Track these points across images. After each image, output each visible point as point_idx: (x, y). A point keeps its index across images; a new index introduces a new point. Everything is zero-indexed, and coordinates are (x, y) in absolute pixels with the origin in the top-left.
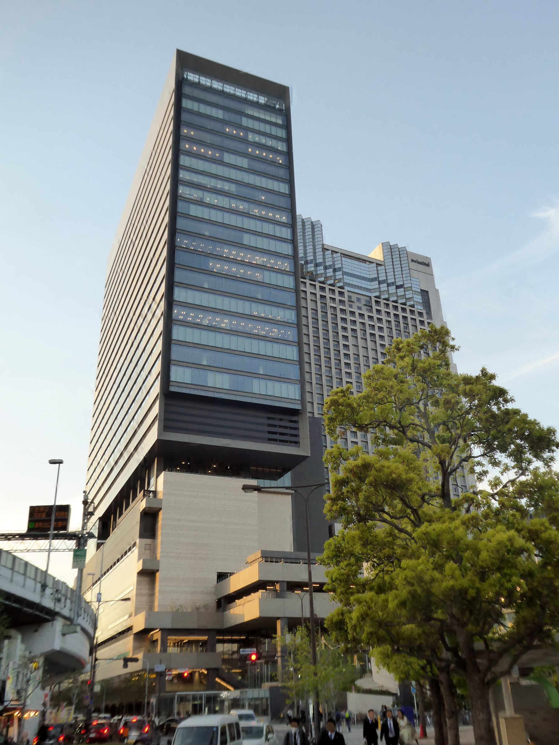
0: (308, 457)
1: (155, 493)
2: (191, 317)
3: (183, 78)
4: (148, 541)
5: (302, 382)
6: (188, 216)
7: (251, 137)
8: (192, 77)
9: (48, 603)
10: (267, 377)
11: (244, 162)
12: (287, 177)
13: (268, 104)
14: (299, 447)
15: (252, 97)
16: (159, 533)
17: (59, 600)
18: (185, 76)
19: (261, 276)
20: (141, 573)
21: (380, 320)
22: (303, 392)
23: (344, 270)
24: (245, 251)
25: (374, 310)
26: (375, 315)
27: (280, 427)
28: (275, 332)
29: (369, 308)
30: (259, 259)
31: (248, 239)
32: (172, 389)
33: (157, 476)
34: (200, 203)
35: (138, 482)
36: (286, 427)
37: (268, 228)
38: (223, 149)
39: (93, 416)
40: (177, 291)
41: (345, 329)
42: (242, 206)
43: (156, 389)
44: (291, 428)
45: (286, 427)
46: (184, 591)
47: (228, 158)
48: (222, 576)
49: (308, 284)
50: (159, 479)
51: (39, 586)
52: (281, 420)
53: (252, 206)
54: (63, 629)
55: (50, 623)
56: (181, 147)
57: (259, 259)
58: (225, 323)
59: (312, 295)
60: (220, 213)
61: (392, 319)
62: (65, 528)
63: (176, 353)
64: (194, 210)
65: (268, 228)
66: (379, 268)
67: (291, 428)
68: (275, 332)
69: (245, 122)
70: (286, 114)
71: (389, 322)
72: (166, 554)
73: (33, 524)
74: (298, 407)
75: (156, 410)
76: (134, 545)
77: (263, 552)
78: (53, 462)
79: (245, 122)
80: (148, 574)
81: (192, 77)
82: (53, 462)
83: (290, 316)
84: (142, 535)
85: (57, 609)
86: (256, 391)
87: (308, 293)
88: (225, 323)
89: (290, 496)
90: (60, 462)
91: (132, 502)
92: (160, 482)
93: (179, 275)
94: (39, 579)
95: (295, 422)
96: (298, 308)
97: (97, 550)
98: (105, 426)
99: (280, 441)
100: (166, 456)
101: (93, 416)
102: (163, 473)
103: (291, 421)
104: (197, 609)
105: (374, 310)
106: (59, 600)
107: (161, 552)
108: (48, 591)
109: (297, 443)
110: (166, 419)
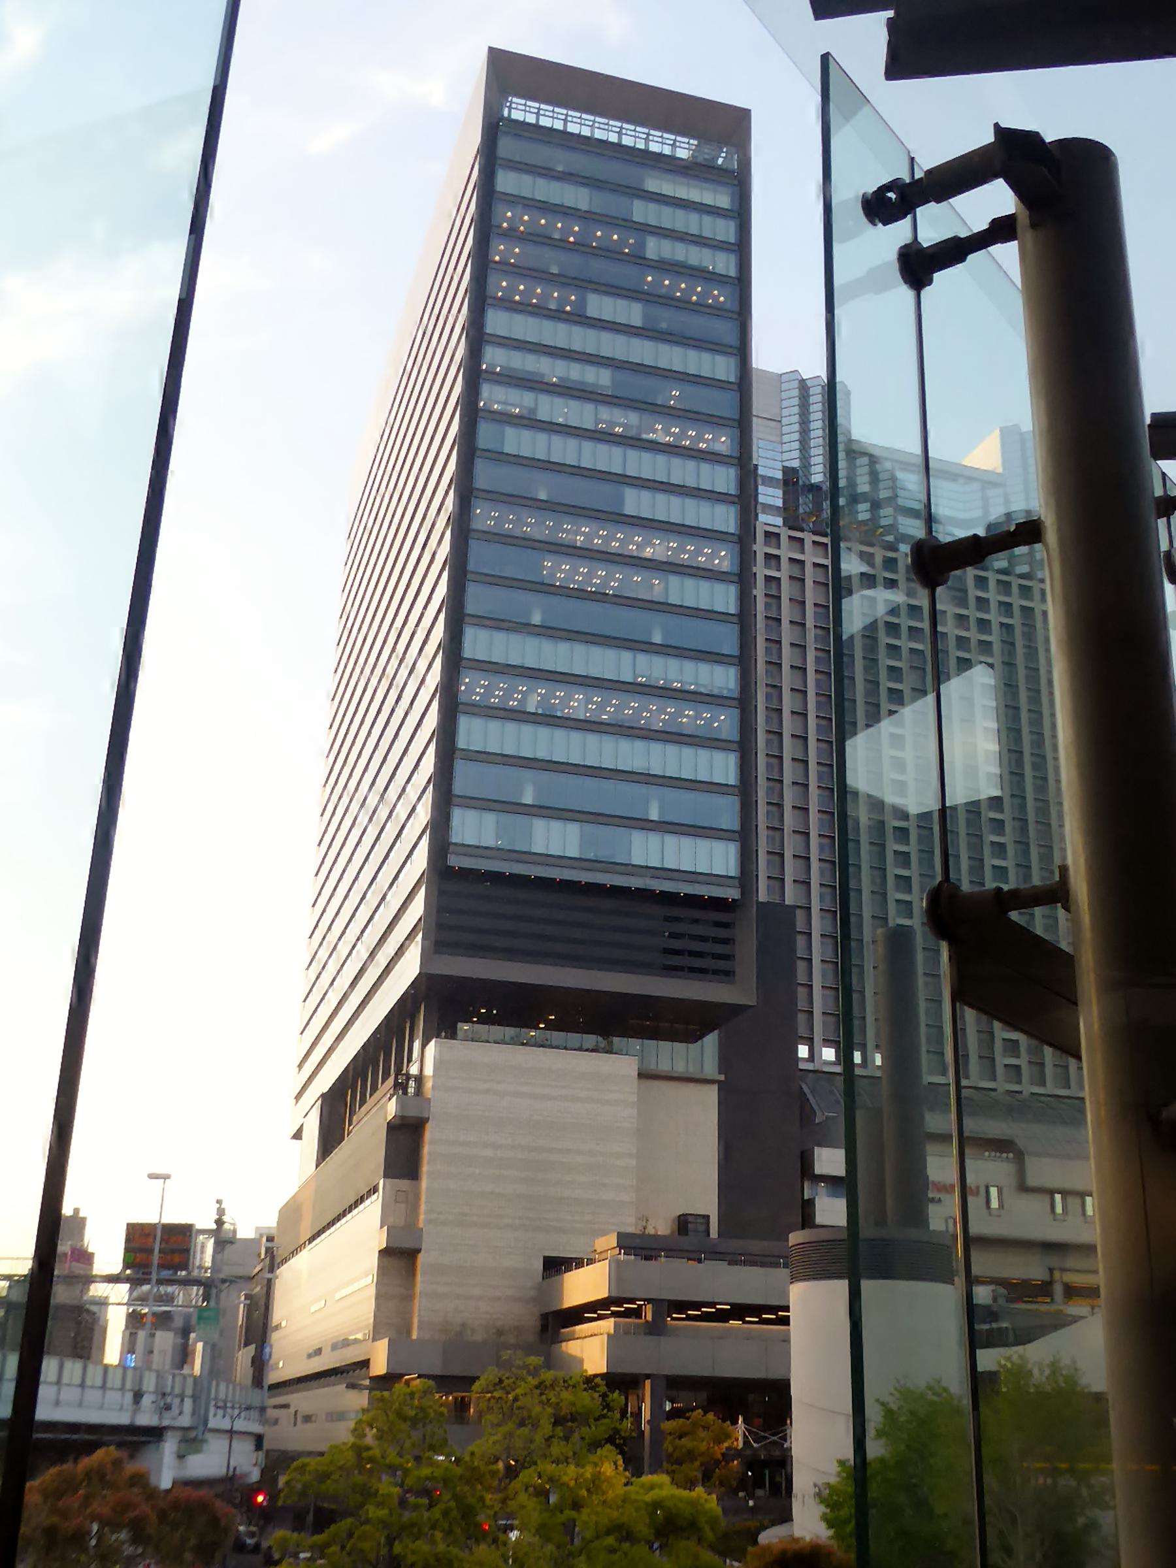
0: (746, 1007)
1: (419, 1079)
2: (499, 692)
3: (502, 118)
4: (404, 1184)
5: (745, 837)
6: (500, 457)
7: (654, 248)
8: (521, 110)
9: (146, 1419)
10: (665, 827)
11: (634, 313)
12: (734, 341)
13: (700, 160)
14: (732, 983)
15: (659, 143)
16: (425, 1168)
17: (168, 1408)
18: (506, 113)
19: (662, 585)
20: (385, 1253)
21: (984, 625)
22: (747, 857)
23: (900, 502)
24: (627, 529)
25: (972, 602)
26: (973, 613)
27: (694, 937)
28: (689, 717)
29: (959, 594)
30: (655, 548)
31: (635, 502)
32: (454, 861)
33: (424, 1046)
34: (529, 422)
35: (382, 1055)
36: (703, 939)
37: (683, 472)
38: (583, 284)
39: (319, 844)
40: (470, 633)
41: (894, 650)
42: (622, 421)
43: (420, 861)
44: (716, 940)
45: (703, 939)
46: (476, 1285)
47: (600, 306)
48: (556, 1266)
49: (808, 545)
50: (428, 1048)
51: (129, 1396)
52: (696, 921)
53: (647, 418)
54: (179, 1448)
55: (153, 1446)
56: (490, 289)
57: (655, 548)
58: (578, 703)
59: (818, 569)
60: (572, 443)
61: (1016, 621)
62: (184, 1266)
63: (465, 779)
64: (517, 441)
65: (683, 472)
66: (991, 493)
67: (716, 940)
68: (689, 717)
69: (641, 211)
70: (739, 182)
71: (1008, 628)
72: (435, 1216)
73: (133, 1255)
74: (732, 894)
75: (418, 908)
76: (375, 1190)
77: (620, 1236)
78: (152, 1176)
79: (641, 211)
80: (400, 1257)
81: (521, 110)
82: (152, 1176)
83: (724, 679)
84: (391, 1171)
85: (165, 1423)
86: (637, 860)
87: (809, 568)
88: (578, 703)
89: (716, 1087)
90: (166, 1177)
91: (371, 1095)
92: (427, 1057)
93: (477, 599)
94: (128, 1385)
95: (726, 925)
96: (744, 661)
97: (317, 1166)
98: (347, 866)
99: (692, 970)
100: (439, 1004)
101: (319, 844)
102: (433, 1043)
103: (718, 924)
104: (500, 1332)
105: (972, 602)
106: (168, 1408)
107: (426, 1213)
108: (147, 1400)
109: (728, 974)
110: (440, 926)
